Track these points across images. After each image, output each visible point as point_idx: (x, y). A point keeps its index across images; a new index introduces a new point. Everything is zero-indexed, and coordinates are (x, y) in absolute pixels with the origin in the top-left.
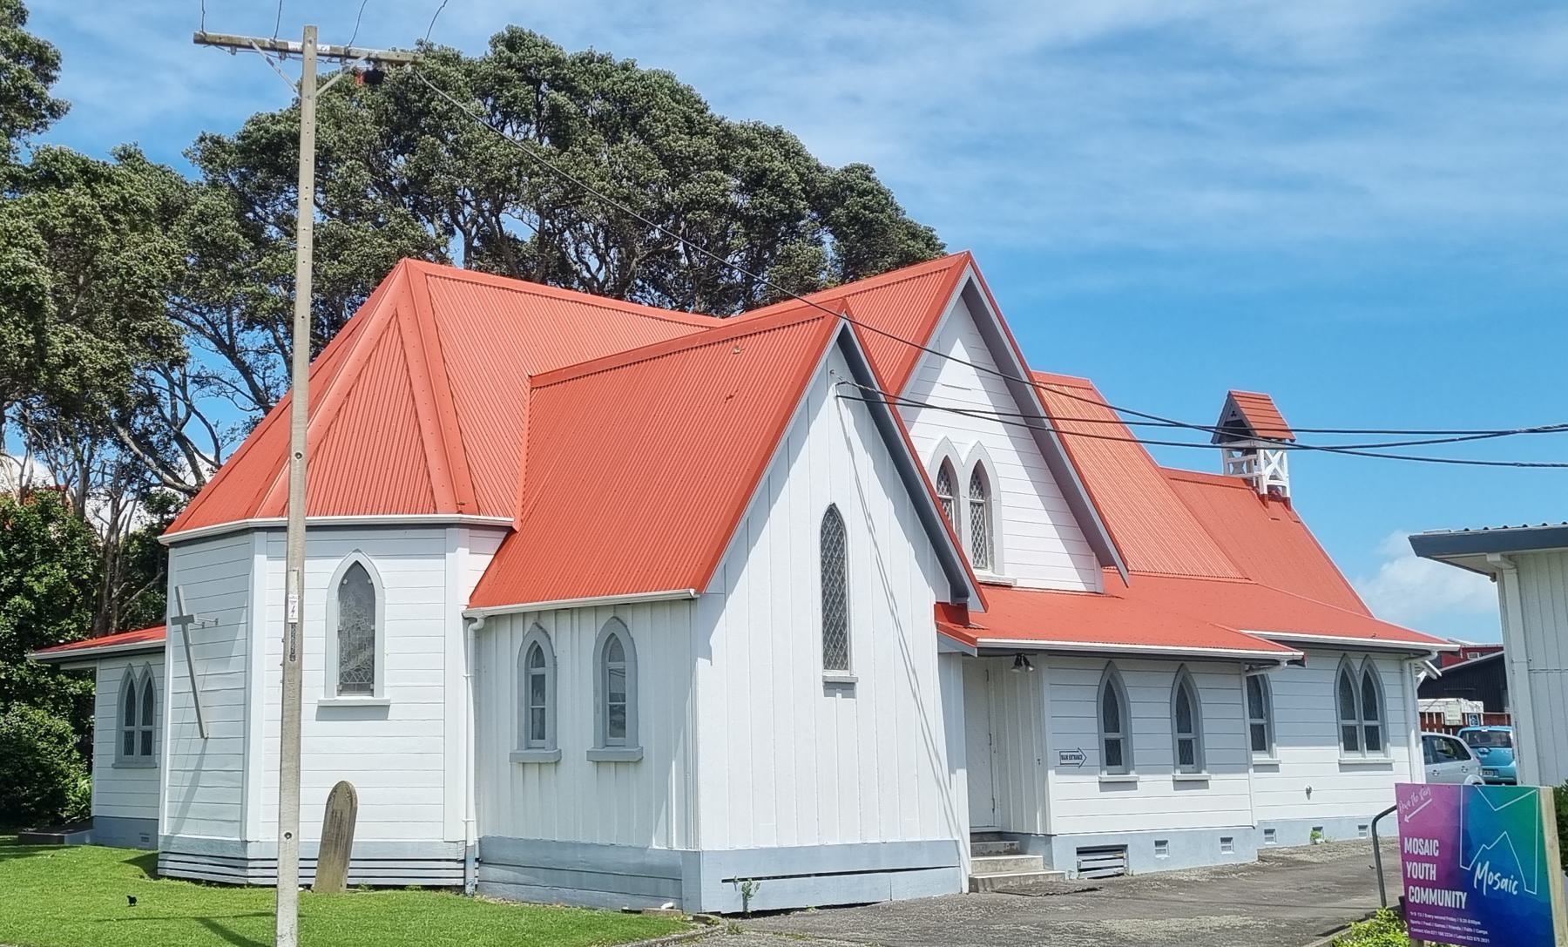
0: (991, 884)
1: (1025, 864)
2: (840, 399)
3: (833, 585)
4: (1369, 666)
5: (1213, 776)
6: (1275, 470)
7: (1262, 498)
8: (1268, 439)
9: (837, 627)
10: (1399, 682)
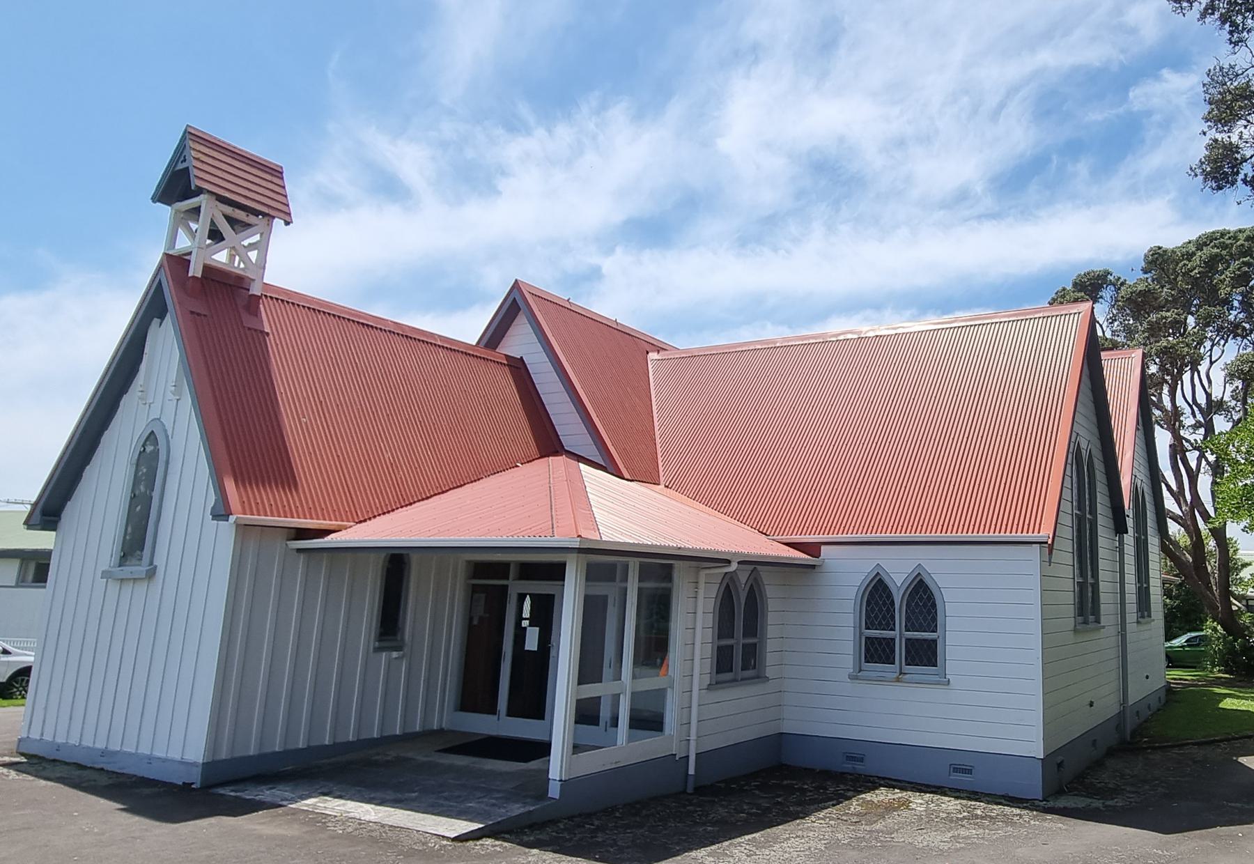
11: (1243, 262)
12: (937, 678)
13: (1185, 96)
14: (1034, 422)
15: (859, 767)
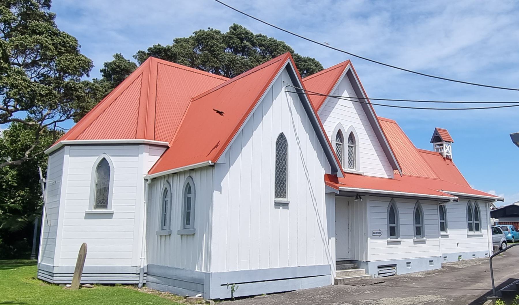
0: (344, 281)
1: (358, 272)
2: (287, 92)
3: (281, 165)
4: (477, 204)
5: (427, 239)
6: (448, 151)
7: (444, 158)
8: (446, 141)
9: (282, 181)
10: (485, 209)
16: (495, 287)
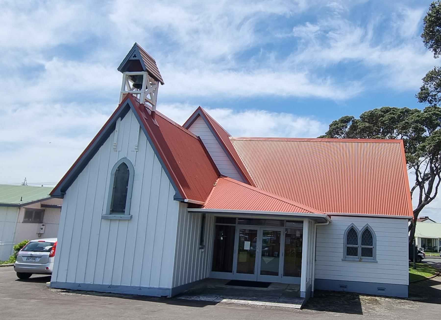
11: (406, 122)
12: (373, 261)
13: (314, 34)
14: (259, 163)
15: (345, 290)
16: (361, 297)
